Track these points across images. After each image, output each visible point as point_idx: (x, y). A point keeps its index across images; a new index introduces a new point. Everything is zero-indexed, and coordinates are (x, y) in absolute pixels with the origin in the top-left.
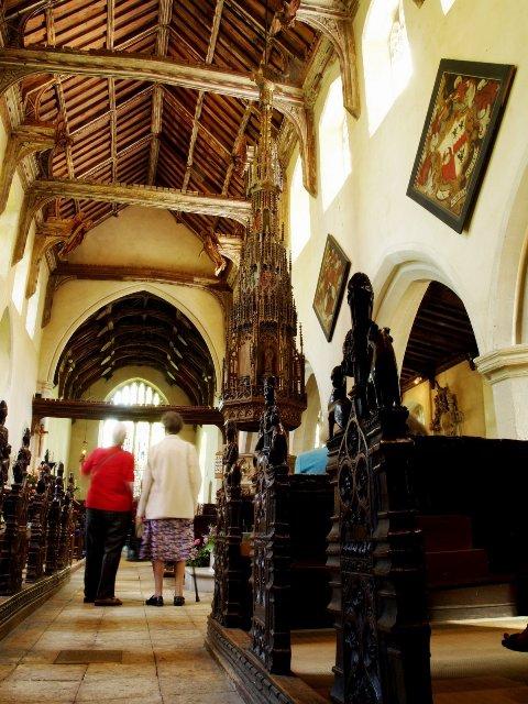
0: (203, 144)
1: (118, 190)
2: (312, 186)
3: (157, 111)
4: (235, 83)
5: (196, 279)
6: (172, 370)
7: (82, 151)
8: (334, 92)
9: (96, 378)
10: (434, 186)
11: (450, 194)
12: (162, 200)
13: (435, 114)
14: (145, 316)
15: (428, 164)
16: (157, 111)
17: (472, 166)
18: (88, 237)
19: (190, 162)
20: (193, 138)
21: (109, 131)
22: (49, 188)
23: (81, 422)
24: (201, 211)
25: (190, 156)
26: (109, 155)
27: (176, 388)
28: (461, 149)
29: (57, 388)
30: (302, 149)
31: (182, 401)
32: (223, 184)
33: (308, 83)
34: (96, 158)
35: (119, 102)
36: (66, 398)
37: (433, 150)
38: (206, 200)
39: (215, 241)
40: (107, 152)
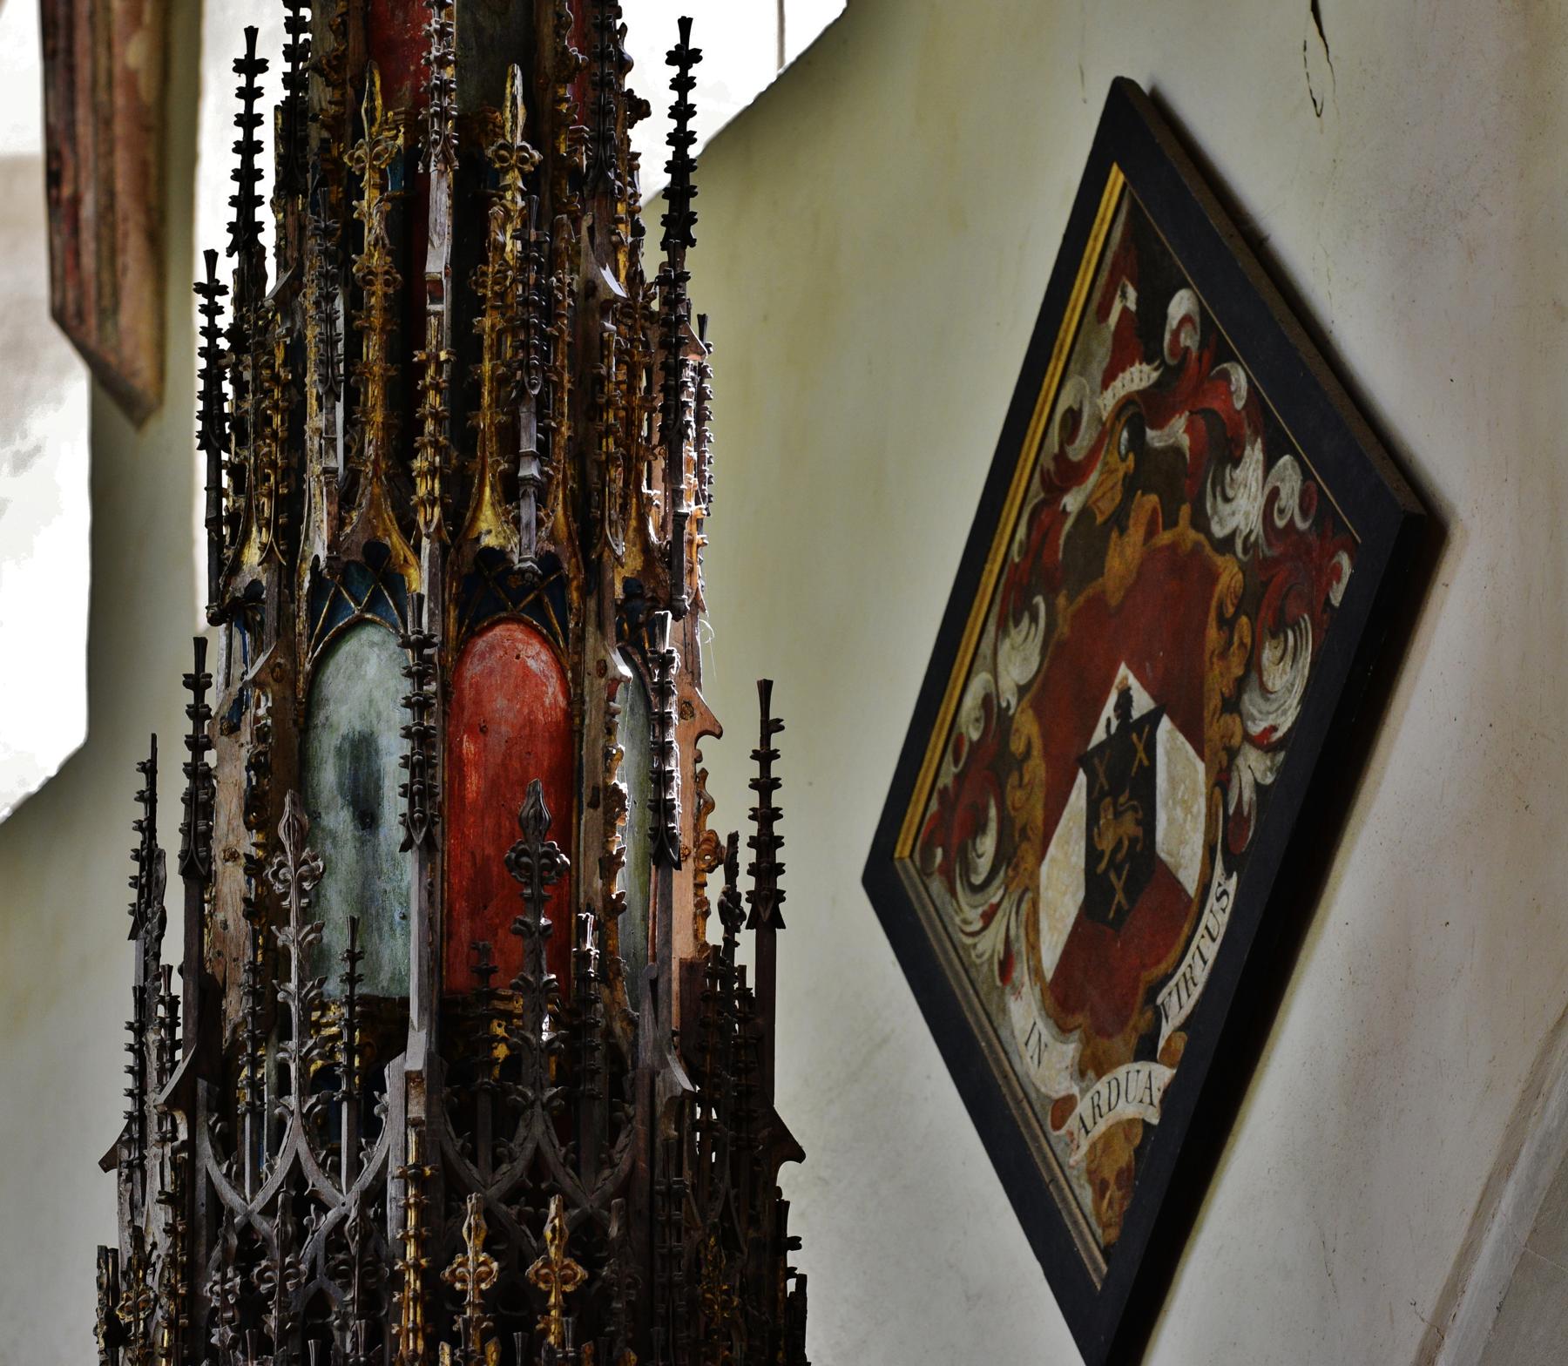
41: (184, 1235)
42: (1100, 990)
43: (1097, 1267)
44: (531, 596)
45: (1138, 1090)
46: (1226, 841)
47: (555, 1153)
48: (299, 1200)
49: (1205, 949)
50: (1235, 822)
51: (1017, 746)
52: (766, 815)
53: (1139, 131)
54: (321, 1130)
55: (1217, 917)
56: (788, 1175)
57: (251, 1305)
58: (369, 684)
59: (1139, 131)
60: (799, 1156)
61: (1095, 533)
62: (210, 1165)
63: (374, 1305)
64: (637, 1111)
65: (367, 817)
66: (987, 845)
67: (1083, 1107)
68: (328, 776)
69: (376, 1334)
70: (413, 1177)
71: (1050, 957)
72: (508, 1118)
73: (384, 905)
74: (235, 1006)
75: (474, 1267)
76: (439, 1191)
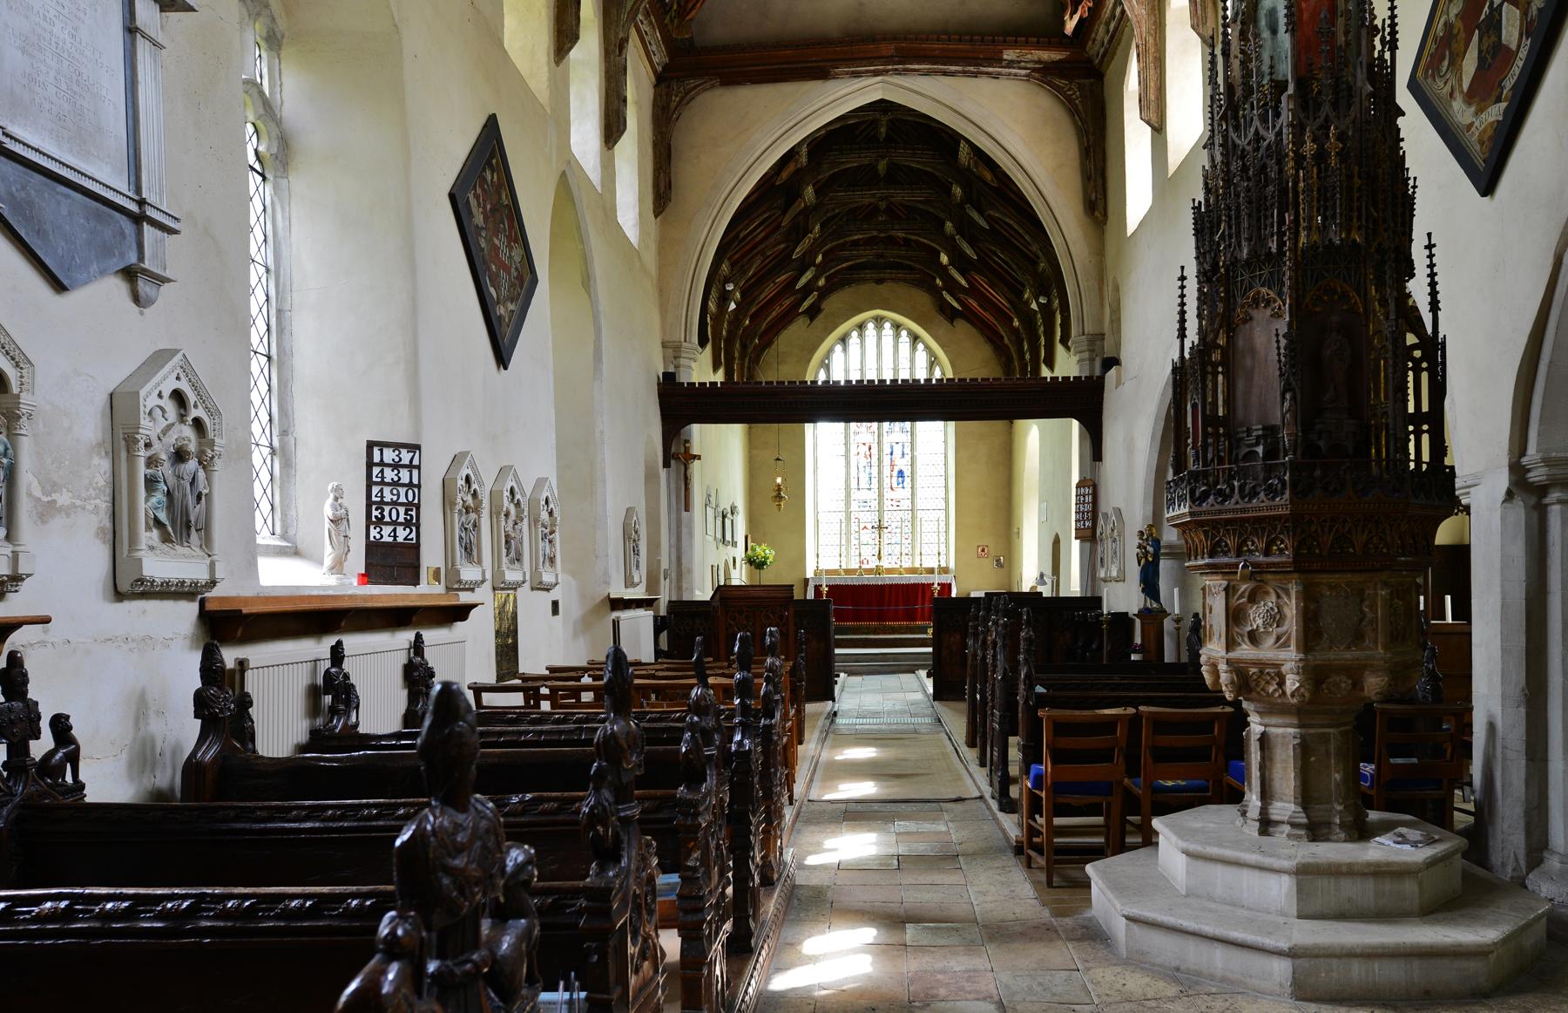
5: (1009, 55)
14: (882, 166)
23: (760, 428)
27: (962, 326)
29: (709, 347)
31: (980, 365)
36: (729, 374)
41: (1225, 155)
42: (1480, 93)
43: (1481, 165)
45: (1495, 112)
46: (1527, 30)
47: (1332, 115)
48: (1258, 138)
49: (1516, 70)
50: (1530, 24)
51: (1455, 31)
52: (1393, 17)
54: (1264, 119)
55: (1523, 54)
56: (1400, 121)
57: (1245, 169)
60: (1403, 114)
62: (1233, 135)
63: (1279, 162)
64: (1357, 100)
65: (1274, 31)
66: (1446, 63)
67: (1477, 124)
68: (1263, 23)
69: (1281, 171)
70: (1291, 125)
71: (1466, 86)
72: (1318, 106)
74: (1239, 92)
76: (1298, 129)
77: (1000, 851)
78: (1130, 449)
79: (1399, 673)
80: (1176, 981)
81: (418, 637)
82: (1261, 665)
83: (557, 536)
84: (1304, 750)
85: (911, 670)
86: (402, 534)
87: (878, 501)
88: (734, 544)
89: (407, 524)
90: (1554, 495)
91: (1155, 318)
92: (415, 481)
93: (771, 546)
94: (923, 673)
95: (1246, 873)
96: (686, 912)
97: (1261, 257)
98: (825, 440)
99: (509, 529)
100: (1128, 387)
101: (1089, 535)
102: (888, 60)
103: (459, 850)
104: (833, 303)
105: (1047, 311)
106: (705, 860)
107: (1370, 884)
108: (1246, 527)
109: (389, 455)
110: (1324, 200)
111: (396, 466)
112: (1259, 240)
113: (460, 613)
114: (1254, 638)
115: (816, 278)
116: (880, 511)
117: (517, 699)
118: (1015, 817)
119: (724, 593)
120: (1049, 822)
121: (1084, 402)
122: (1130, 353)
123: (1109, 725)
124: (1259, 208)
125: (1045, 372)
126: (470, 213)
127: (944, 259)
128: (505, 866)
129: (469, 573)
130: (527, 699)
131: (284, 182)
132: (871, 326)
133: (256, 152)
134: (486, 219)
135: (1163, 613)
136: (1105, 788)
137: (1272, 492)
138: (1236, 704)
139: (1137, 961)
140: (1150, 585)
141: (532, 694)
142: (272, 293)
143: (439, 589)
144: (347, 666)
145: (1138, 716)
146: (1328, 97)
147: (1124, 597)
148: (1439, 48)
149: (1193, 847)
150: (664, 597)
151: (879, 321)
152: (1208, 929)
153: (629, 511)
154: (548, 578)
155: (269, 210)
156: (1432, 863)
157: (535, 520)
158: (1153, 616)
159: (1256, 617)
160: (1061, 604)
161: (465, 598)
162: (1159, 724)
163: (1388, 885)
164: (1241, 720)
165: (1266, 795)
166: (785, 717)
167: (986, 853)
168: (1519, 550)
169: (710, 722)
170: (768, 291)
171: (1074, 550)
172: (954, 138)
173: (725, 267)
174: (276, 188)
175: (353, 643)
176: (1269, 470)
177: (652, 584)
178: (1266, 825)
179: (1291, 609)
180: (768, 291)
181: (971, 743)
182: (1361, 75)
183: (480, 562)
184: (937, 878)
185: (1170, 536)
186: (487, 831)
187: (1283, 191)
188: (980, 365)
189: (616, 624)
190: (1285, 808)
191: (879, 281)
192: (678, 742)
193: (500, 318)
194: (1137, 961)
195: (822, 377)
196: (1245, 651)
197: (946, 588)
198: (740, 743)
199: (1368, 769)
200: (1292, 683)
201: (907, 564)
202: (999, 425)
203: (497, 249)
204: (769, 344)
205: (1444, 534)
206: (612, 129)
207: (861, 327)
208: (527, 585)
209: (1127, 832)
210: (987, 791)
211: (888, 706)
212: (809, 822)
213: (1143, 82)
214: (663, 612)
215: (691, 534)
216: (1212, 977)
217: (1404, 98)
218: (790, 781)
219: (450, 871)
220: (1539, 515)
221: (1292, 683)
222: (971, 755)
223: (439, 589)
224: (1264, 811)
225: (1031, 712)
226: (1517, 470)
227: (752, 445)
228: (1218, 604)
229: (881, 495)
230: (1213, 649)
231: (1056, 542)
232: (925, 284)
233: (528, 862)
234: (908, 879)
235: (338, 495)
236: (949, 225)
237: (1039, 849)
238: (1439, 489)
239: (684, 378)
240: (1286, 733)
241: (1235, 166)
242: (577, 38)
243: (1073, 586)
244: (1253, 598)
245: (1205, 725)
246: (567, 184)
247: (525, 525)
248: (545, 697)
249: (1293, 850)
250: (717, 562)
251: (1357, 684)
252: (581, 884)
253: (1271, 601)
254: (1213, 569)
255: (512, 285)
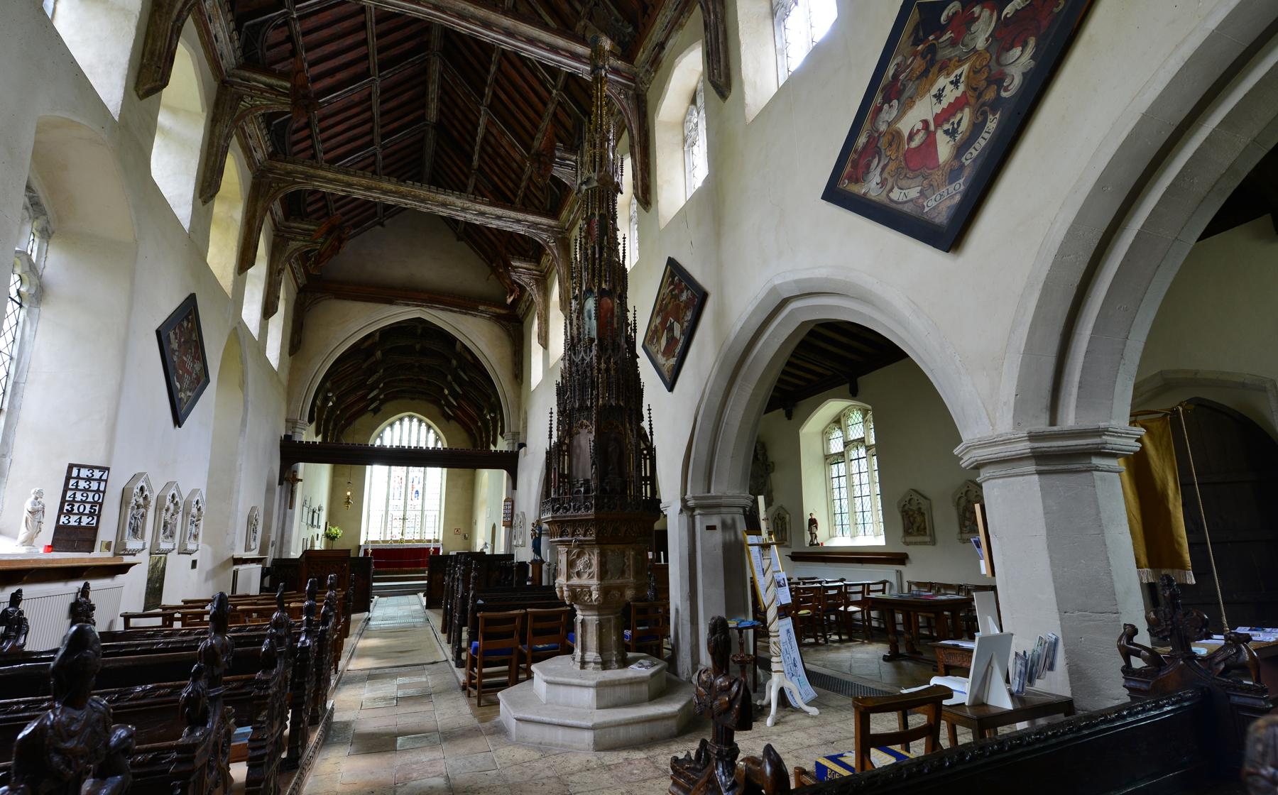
0: (492, 140)
1: (386, 186)
2: (645, 194)
3: (433, 91)
4: (548, 44)
5: (481, 308)
6: (450, 405)
7: (325, 33)
8: (688, 68)
9: (362, 412)
10: (883, 183)
11: (921, 192)
12: (444, 205)
13: (891, 71)
14: (418, 347)
15: (873, 148)
16: (433, 91)
17: (981, 143)
18: (348, 247)
19: (475, 163)
20: (481, 131)
21: (370, 108)
22: (289, 173)
23: (339, 466)
24: (494, 224)
25: (476, 157)
26: (371, 143)
27: (453, 423)
28: (959, 116)
29: (314, 425)
30: (632, 147)
31: (462, 443)
32: (516, 196)
33: (642, 56)
34: (353, 145)
35: (382, 66)
36: (324, 438)
37: (883, 128)
38: (499, 211)
39: (507, 265)
40: (367, 139)
42: (668, 352)
44: (609, 294)
45: (673, 361)
46: (683, 333)
48: (583, 359)
53: (671, 262)
58: (590, 304)
59: (671, 262)
61: (667, 305)
73: (592, 326)
75: (603, 366)
76: (599, 358)
77: (455, 689)
78: (529, 484)
79: (639, 588)
80: (540, 750)
81: (86, 586)
82: (582, 587)
83: (202, 523)
84: (600, 626)
85: (415, 593)
86: (85, 521)
87: (402, 504)
88: (319, 527)
89: (91, 514)
90: (697, 512)
91: (540, 425)
92: (102, 488)
93: (341, 528)
94: (421, 595)
95: (574, 690)
96: (253, 749)
97: (583, 408)
98: (376, 475)
99: (168, 518)
100: (529, 457)
101: (509, 524)
102: (423, 301)
103: (71, 736)
104: (387, 407)
105: (494, 420)
106: (270, 717)
107: (628, 689)
108: (576, 524)
109: (84, 473)
110: (608, 386)
111: (89, 479)
112: (583, 401)
113: (124, 569)
114: (579, 574)
115: (379, 395)
116: (405, 511)
117: (158, 621)
118: (463, 670)
119: (309, 554)
120: (480, 671)
121: (509, 463)
122: (530, 442)
123: (512, 619)
124: (583, 388)
125: (492, 448)
126: (169, 342)
127: (446, 392)
128: (109, 741)
129: (132, 544)
130: (164, 622)
131: (36, 310)
132: (406, 419)
133: (18, 291)
134: (179, 346)
135: (542, 561)
136: (510, 651)
137: (587, 508)
138: (571, 605)
139: (521, 742)
140: (537, 549)
141: (168, 618)
142: (12, 372)
143: (109, 554)
144: (22, 606)
145: (527, 614)
146: (610, 347)
147: (524, 554)
148: (652, 335)
149: (550, 678)
150: (270, 557)
151: (411, 418)
152: (555, 720)
153: (253, 509)
154: (191, 547)
155: (21, 324)
156: (653, 675)
157: (187, 513)
158: (538, 563)
159: (580, 565)
160: (494, 557)
161: (127, 560)
162: (537, 617)
163: (635, 688)
164: (573, 613)
165: (584, 649)
166: (338, 622)
167: (445, 691)
168: (685, 534)
169: (282, 632)
170: (352, 399)
171: (502, 532)
172: (454, 340)
173: (328, 385)
174: (29, 312)
175: (29, 590)
176: (586, 499)
177: (263, 549)
178: (583, 664)
179: (595, 561)
180: (352, 399)
181: (444, 631)
182: (623, 341)
183: (142, 538)
184: (418, 708)
185: (545, 526)
186: (98, 721)
187: (593, 382)
188: (462, 443)
189: (235, 573)
190: (592, 655)
191: (413, 399)
192: (261, 643)
193: (181, 399)
194: (521, 742)
195: (378, 443)
196: (575, 581)
197: (437, 550)
198: (304, 642)
199: (628, 633)
200: (595, 595)
201: (417, 537)
202: (468, 471)
203: (184, 362)
204: (350, 424)
205: (657, 526)
206: (268, 310)
207: (401, 420)
208: (176, 551)
209: (519, 674)
210: (450, 656)
211: (400, 613)
212: (345, 683)
213: (540, 328)
214: (268, 565)
215: (292, 522)
216: (557, 745)
217: (640, 351)
218: (338, 658)
219: (58, 751)
220: (692, 517)
221: (595, 595)
222: (443, 637)
223: (109, 554)
224: (582, 657)
225: (474, 611)
226: (684, 501)
227: (334, 476)
228: (563, 559)
229: (405, 503)
230: (561, 580)
231: (494, 527)
232: (436, 402)
233: (130, 736)
234: (401, 710)
235: (39, 495)
236: (449, 377)
237: (474, 686)
238: (653, 507)
239: (297, 439)
240: (592, 619)
241: (574, 369)
242: (253, 264)
243: (500, 550)
244: (579, 556)
245: (557, 616)
246: (239, 329)
247: (179, 516)
248: (178, 619)
249: (595, 675)
250: (306, 534)
251: (622, 595)
252: (174, 743)
253: (586, 557)
254: (562, 543)
255: (192, 382)
